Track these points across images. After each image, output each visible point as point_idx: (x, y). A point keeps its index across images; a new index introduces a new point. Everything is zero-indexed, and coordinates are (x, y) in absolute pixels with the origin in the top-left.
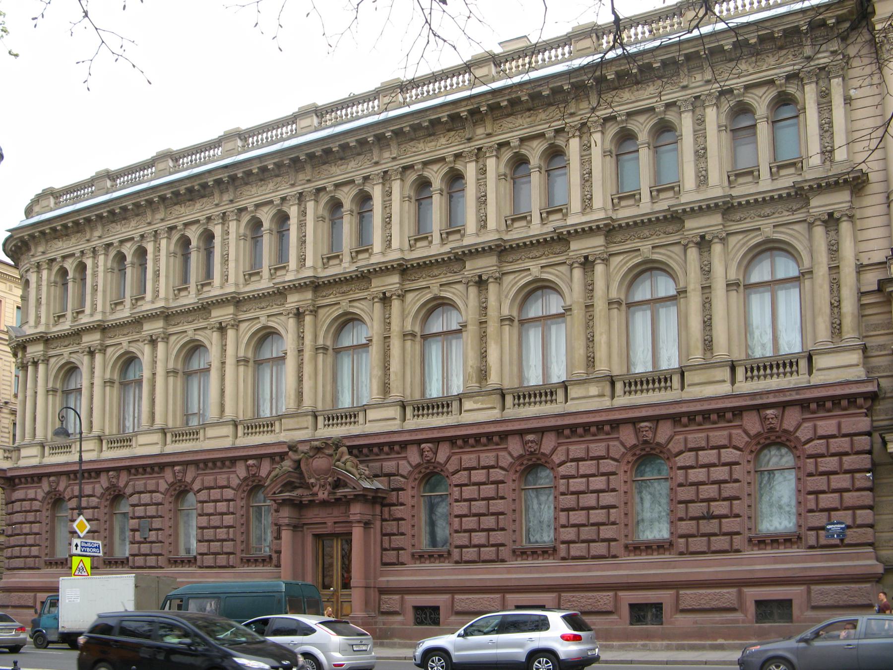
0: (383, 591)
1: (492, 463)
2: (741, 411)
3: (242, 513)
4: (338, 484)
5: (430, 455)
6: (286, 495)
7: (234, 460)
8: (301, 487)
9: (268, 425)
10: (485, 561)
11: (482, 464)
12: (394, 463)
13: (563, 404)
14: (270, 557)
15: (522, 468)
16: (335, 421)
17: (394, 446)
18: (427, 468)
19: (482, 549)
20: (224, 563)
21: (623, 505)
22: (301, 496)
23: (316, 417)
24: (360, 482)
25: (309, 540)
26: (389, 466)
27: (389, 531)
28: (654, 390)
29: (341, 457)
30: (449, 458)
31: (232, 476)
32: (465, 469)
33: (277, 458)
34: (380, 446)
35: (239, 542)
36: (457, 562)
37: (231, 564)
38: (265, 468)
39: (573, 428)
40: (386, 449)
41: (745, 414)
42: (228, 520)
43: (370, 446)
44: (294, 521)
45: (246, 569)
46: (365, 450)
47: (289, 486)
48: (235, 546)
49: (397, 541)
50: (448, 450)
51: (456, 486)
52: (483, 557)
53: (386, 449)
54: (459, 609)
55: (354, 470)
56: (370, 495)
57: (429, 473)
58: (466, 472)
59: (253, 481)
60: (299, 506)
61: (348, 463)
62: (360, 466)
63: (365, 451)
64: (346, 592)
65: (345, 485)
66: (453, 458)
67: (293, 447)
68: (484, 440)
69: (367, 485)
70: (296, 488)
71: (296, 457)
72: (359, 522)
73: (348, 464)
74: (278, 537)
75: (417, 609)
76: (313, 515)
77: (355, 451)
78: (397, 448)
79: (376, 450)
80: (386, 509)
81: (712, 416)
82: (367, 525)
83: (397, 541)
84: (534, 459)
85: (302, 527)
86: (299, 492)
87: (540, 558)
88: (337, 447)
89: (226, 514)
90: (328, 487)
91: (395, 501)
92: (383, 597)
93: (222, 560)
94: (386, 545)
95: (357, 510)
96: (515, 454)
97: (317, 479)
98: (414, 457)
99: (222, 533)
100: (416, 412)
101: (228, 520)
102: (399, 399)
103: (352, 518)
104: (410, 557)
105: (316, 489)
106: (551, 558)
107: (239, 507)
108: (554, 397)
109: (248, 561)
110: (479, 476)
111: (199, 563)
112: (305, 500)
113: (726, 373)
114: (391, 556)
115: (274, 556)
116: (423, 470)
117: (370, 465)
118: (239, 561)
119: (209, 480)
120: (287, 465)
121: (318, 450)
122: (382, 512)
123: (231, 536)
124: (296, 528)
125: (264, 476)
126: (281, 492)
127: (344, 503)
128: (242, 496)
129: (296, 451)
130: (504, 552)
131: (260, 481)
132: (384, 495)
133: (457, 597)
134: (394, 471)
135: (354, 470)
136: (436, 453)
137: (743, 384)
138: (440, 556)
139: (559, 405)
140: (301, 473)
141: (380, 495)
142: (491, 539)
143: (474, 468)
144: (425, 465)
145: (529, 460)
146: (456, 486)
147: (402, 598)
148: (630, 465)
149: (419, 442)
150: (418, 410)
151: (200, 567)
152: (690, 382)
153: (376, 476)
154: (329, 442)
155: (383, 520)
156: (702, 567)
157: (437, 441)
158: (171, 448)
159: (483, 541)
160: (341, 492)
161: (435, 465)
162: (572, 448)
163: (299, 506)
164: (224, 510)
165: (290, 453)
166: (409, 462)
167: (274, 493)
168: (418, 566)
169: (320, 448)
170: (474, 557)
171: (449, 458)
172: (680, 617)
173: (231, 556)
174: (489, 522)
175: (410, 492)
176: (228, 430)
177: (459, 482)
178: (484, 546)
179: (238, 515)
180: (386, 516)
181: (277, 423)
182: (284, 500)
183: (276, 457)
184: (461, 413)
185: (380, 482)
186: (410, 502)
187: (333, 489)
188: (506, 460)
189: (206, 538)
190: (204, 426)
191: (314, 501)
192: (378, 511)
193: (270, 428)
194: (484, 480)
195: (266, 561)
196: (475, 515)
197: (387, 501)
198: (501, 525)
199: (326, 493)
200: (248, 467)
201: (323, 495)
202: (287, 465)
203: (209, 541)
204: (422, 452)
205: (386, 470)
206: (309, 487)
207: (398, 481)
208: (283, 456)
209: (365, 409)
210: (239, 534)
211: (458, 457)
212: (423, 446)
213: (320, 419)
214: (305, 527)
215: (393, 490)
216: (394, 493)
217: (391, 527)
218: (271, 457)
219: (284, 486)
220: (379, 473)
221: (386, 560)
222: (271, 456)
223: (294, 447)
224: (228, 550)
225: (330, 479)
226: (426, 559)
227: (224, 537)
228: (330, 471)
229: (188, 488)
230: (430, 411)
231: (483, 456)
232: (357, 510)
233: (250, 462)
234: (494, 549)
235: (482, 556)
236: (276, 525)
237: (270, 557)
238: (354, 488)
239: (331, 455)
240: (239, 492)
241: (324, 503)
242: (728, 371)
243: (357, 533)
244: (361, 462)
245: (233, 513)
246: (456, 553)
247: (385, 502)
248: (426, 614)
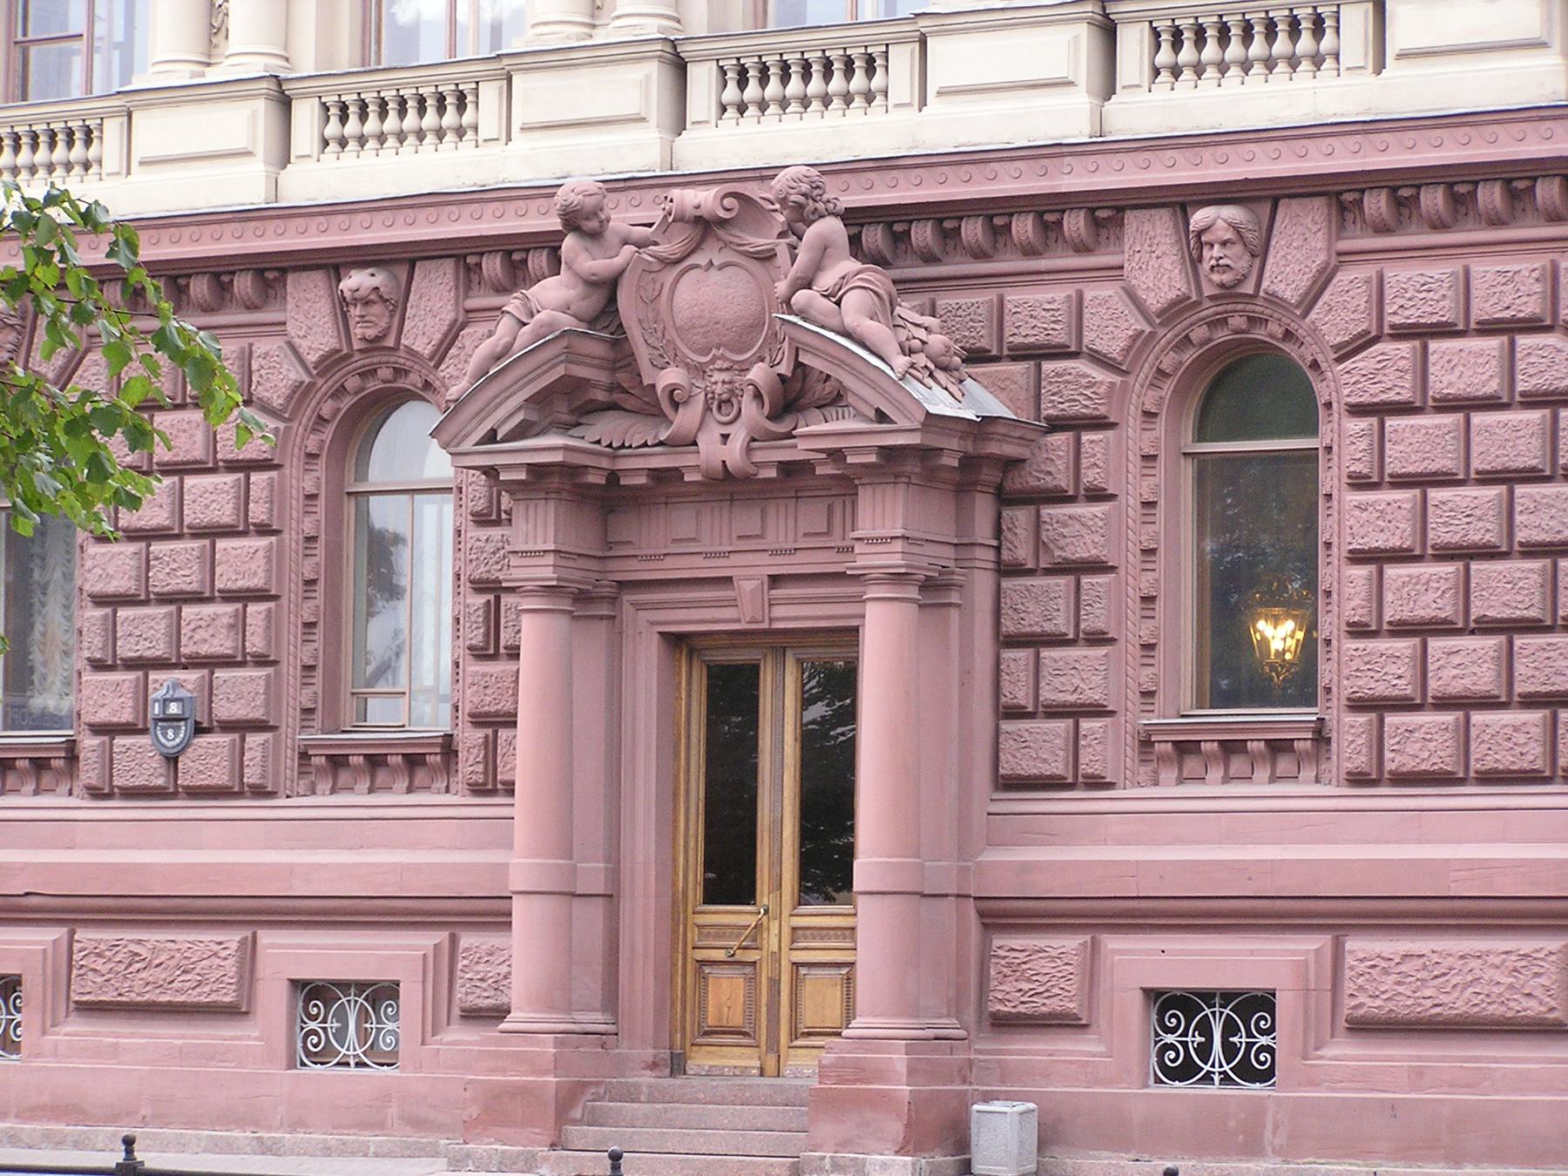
0: (1000, 916)
1: (1530, 307)
2: (1120, 210)
3: (308, 527)
4: (794, 396)
5: (1237, 258)
6: (549, 446)
7: (273, 273)
8: (613, 407)
9: (445, 103)
10: (1491, 778)
11: (1483, 309)
12: (1058, 294)
13: (1368, 77)
14: (448, 747)
15: (1189, 356)
16: (411, 120)
17: (1072, 219)
18: (1219, 322)
19: (1477, 717)
20: (220, 777)
21: (1135, 558)
22: (615, 451)
23: (679, 67)
24: (914, 388)
25: (646, 656)
26: (1035, 309)
27: (1032, 623)
28: (1270, 64)
29: (818, 266)
30: (1323, 279)
31: (262, 346)
32: (1402, 333)
33: (493, 266)
34: (995, 212)
35: (290, 670)
36: (1358, 780)
37: (252, 776)
38: (433, 301)
39: (1402, 188)
40: (1023, 227)
41: (290, 278)
42: (242, 562)
43: (945, 215)
44: (578, 574)
45: (324, 802)
46: (917, 233)
47: (565, 402)
48: (273, 691)
49: (1074, 674)
50: (1319, 241)
51: (1358, 410)
52: (1484, 756)
53: (973, 230)
54: (1372, 1006)
55: (875, 330)
56: (952, 450)
57: (1225, 348)
58: (1405, 347)
59: (1219, 322)
60: (601, 498)
61: (852, 300)
62: (905, 310)
63: (922, 234)
64: (819, 915)
65: (837, 399)
66: (1343, 278)
67: (582, 221)
68: (1491, 196)
69: (941, 403)
70: (586, 411)
71: (598, 265)
72: (898, 578)
73: (849, 300)
74: (492, 647)
75: (1173, 1005)
76: (675, 543)
77: (874, 237)
78: (1075, 223)
79: (973, 230)
80: (1020, 517)
81: (1482, 193)
82: (933, 589)
83: (1074, 674)
84: (1237, 321)
85: (613, 600)
86: (607, 428)
87: (1263, 773)
88: (800, 215)
89: (230, 532)
90: (749, 407)
91: (1063, 481)
92: (1001, 941)
93: (208, 759)
94: (1018, 692)
95: (885, 524)
96: (1155, 301)
97: (700, 371)
98: (1153, 263)
99: (207, 628)
100: (1165, 56)
101: (242, 562)
102: (652, 29)
103: (866, 559)
104: (1131, 751)
105: (686, 419)
106: (1308, 773)
107: (296, 504)
108: (1327, 43)
109: (337, 763)
110: (1465, 365)
111: (89, 773)
112: (636, 467)
113: (640, 85)
114: (1041, 745)
115: (470, 739)
116: (1198, 334)
117: (945, 301)
118: (290, 761)
119: (1421, 288)
121: (705, 227)
122: (998, 532)
123: (256, 643)
124: (589, 599)
125: (1290, 294)
126: (520, 432)
127: (826, 484)
128: (312, 445)
129: (595, 236)
130: (1102, 745)
131: (400, 372)
132: (1010, 450)
133: (1358, 946)
134: (1061, 335)
135: (875, 330)
136: (1260, 254)
137: (1141, 95)
138: (1278, 748)
139: (896, 115)
140: (619, 341)
141: (994, 448)
142: (1520, 669)
143: (1445, 331)
144: (1209, 310)
145: (341, 391)
146: (1358, 410)
147: (1095, 947)
148: (1168, 386)
149: (1181, 201)
150: (742, 83)
151: (96, 793)
152: (949, 82)
153: (976, 356)
154: (753, 190)
155: (1007, 570)
156: (1154, 842)
157: (1265, 196)
158: (1152, 106)
159: (1484, 679)
160: (817, 432)
161: (1258, 308)
162: (1400, 275)
163: (601, 498)
164: (223, 512)
165: (569, 243)
166: (1131, 294)
167: (491, 437)
168: (1170, 792)
169: (727, 219)
170: (1440, 755)
171: (1323, 279)
172: (1345, 1053)
173: (254, 740)
174: (1507, 587)
175: (1134, 436)
176: (247, 121)
177: (1373, 393)
178: (1488, 703)
179: (291, 539)
180: (1021, 551)
181: (490, 94)
182: (538, 472)
183: (496, 261)
184: (1380, 66)
185: (997, 387)
186: (1133, 486)
187: (774, 416)
188: (1111, 323)
189: (126, 649)
190: (130, 102)
191: (676, 473)
192: (983, 530)
193: (78, 151)
194: (1492, 387)
195: (422, 762)
196: (1446, 554)
197: (1031, 479)
198: (1093, 620)
199: (739, 435)
200: (342, 305)
201: (722, 446)
202: (552, 296)
203: (142, 665)
204: (1194, 247)
205: (1022, 331)
206: (652, 406)
207: (1074, 385)
208: (519, 258)
209: (505, 68)
210: (291, 632)
211: (1369, 271)
212: (1200, 217)
213: (305, 114)
214: (628, 598)
215: (1056, 425)
216: (1060, 439)
217: (1043, 602)
218: (460, 258)
219: (540, 400)
220: (986, 342)
221: (1016, 763)
222: (462, 256)
223: (595, 212)
224: (240, 711)
225: (758, 373)
226: (1207, 761)
227: (222, 644)
228: (747, 335)
229: (413, 381)
230: (1235, 49)
231: (1484, 270)
232: (885, 524)
233: (357, 280)
234: (1535, 716)
235: (1476, 750)
236: (480, 586)
237: (448, 747)
238: (881, 417)
239: (767, 257)
240: (298, 427)
241: (728, 487)
242: (652, 73)
243: (884, 638)
244: (905, 286)
245: (264, 530)
246: (1350, 732)
247: (1017, 482)
248: (1205, 1029)
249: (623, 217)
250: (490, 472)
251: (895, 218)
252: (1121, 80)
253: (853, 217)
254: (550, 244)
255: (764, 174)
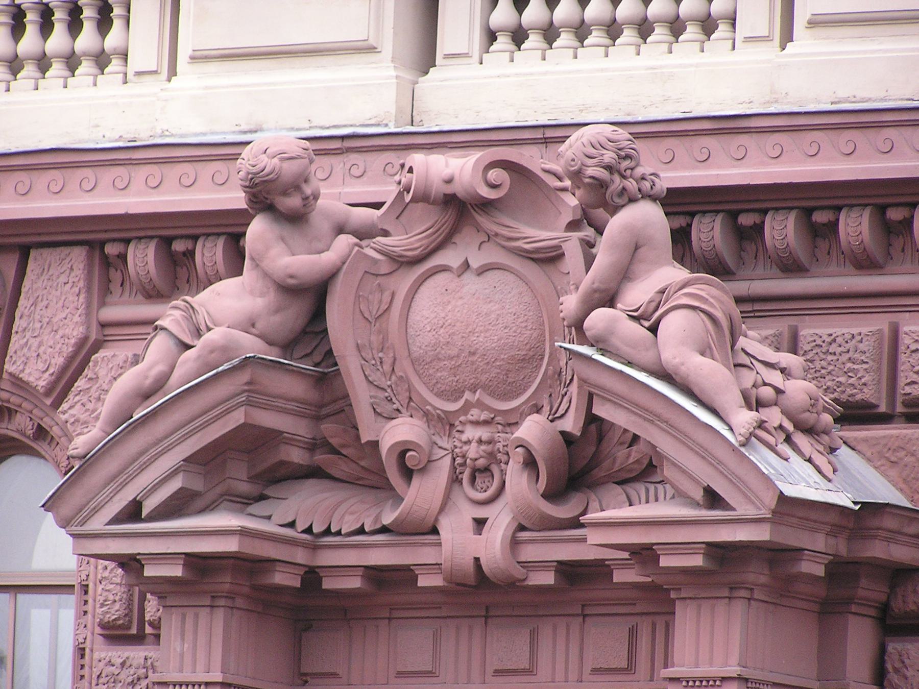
62: (753, 342)
86: (304, 505)
108: (113, 39)
117: (813, 330)
120: (230, 307)
121: (459, 211)
126: (177, 506)
129: (296, 219)
140: (327, 376)
153: (855, 414)
167: (133, 512)
191: (403, 576)
202: (230, 307)
219: (207, 460)
249: (339, 192)
250: (130, 564)
251: (740, 207)
252: (447, 42)
253: (682, 204)
254: (229, 229)
255: (550, 135)
